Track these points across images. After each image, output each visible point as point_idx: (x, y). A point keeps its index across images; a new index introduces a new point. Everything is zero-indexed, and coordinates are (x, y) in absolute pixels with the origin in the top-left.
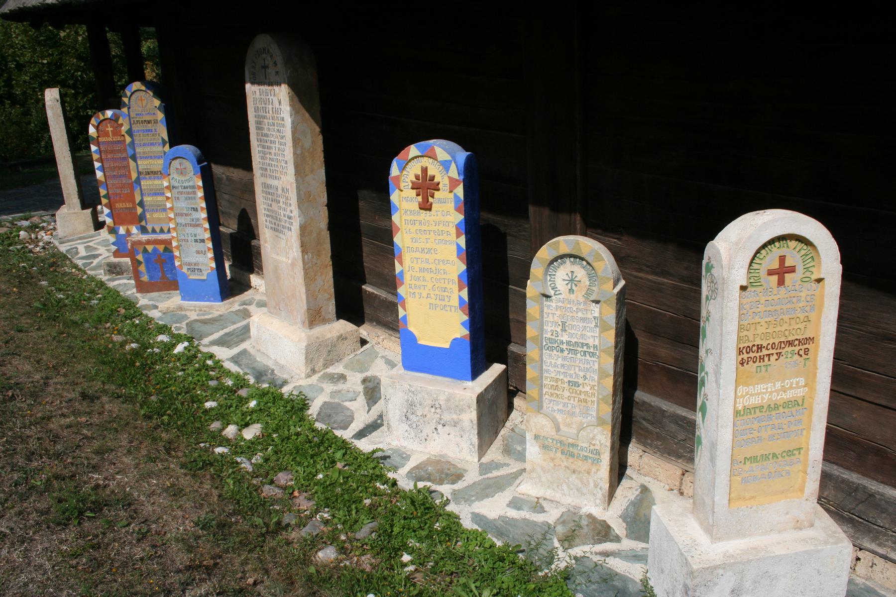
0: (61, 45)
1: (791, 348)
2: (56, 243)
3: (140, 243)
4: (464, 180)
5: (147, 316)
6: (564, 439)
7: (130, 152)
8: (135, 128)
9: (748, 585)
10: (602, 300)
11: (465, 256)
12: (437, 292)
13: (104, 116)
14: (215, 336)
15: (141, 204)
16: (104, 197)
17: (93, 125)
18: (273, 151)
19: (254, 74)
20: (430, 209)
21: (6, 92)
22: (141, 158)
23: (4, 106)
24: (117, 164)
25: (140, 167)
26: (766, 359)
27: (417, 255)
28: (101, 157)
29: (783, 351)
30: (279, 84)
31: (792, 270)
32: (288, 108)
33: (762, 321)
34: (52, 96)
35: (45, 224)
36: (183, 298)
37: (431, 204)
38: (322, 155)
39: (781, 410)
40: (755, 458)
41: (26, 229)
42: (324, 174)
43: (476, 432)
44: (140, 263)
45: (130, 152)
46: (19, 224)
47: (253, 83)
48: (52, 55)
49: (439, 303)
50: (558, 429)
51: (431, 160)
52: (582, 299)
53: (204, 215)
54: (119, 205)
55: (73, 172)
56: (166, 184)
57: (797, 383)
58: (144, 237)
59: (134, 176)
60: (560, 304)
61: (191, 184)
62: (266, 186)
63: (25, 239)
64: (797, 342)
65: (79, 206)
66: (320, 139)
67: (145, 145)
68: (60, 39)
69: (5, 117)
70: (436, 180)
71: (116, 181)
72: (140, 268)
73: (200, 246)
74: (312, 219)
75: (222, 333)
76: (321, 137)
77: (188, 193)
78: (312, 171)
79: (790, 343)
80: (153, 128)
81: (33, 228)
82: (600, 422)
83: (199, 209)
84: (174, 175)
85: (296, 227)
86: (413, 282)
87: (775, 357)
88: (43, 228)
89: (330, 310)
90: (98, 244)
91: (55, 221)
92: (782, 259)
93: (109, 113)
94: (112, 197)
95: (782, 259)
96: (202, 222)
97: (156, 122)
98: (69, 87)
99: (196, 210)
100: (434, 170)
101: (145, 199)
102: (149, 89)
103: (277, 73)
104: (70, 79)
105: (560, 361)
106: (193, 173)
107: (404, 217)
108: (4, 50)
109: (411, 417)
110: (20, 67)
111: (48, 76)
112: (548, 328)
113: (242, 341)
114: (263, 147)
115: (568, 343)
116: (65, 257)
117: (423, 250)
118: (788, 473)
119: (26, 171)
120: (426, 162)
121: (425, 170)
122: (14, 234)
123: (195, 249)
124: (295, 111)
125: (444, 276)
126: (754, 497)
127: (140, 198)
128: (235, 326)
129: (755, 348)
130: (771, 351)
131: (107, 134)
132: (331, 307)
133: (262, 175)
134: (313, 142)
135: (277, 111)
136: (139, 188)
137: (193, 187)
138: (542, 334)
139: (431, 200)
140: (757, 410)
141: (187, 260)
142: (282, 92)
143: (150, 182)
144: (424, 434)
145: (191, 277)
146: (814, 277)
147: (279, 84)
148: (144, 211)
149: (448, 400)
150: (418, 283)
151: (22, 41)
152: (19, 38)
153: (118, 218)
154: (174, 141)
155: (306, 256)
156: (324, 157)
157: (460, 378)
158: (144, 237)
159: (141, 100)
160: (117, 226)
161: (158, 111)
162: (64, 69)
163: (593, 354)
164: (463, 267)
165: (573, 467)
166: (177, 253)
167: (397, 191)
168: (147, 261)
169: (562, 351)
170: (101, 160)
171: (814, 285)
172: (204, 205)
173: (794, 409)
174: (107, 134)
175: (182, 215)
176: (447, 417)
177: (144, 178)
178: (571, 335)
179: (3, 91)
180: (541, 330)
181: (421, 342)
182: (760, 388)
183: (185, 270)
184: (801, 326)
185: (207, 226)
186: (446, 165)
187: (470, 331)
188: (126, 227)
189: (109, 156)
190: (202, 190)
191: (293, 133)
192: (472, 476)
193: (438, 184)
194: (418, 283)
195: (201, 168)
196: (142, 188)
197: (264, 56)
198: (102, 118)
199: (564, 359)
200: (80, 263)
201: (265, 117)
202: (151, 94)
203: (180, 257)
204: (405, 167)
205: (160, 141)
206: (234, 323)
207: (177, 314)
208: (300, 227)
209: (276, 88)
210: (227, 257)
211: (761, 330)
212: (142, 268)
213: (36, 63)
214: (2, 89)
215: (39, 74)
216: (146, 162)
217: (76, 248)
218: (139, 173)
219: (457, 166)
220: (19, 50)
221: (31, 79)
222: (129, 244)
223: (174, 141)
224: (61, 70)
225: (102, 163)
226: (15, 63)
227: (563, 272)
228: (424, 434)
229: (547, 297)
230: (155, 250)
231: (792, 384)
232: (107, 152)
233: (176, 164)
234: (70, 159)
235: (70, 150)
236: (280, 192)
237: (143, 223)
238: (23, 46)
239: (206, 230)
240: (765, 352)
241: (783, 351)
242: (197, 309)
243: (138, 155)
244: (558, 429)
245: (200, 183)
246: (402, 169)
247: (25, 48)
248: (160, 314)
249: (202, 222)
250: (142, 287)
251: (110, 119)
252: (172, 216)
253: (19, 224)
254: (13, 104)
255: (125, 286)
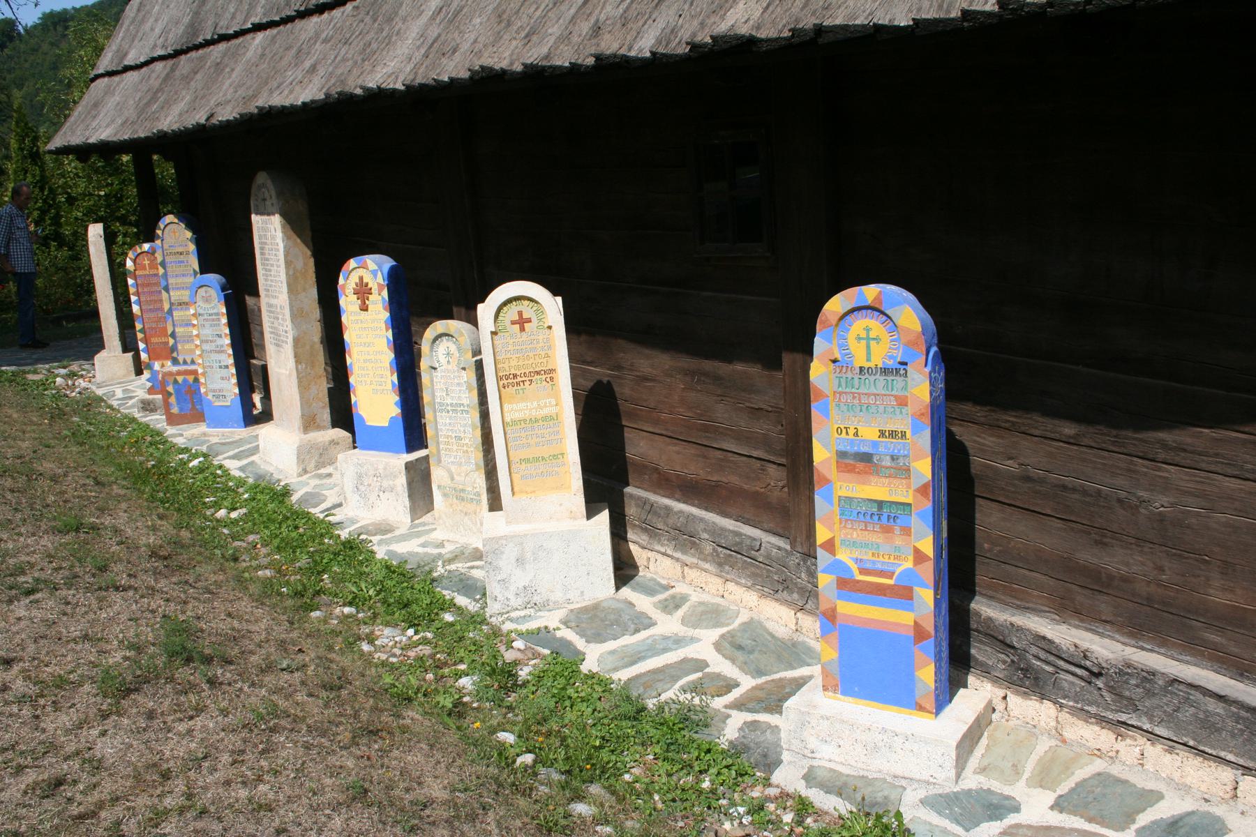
0: (124, 171)
1: (539, 377)
2: (94, 388)
3: (170, 374)
4: (388, 285)
5: (171, 442)
6: (456, 486)
7: (163, 283)
8: (168, 259)
9: (528, 555)
10: (467, 367)
11: (392, 347)
12: (376, 379)
13: (141, 249)
14: (231, 453)
15: (173, 335)
16: (140, 331)
17: (131, 259)
18: (272, 273)
19: (257, 206)
20: (367, 310)
21: (52, 232)
22: (173, 289)
23: (49, 248)
24: (152, 298)
25: (172, 298)
26: (522, 384)
27: (361, 348)
28: (138, 290)
29: (534, 379)
30: (273, 214)
31: (529, 321)
32: (281, 235)
33: (514, 357)
34: (95, 232)
35: (84, 373)
36: (209, 426)
37: (367, 306)
38: (314, 276)
39: (541, 423)
40: (528, 460)
41: (62, 377)
42: (316, 293)
43: (407, 495)
44: (170, 394)
45: (163, 283)
46: (56, 372)
47: (257, 214)
48: (112, 184)
49: (379, 388)
50: (452, 479)
51: (365, 270)
52: (456, 369)
53: (228, 341)
54: (155, 340)
55: (114, 312)
56: (192, 311)
57: (550, 403)
58: (175, 369)
59: (166, 307)
60: (443, 374)
61: (215, 311)
62: (270, 306)
63: (60, 385)
64: (543, 372)
65: (120, 349)
66: (311, 262)
67: (177, 276)
68: (122, 164)
69: (50, 262)
70: (369, 286)
71: (152, 315)
72: (170, 400)
73: (224, 372)
74: (305, 333)
75: (237, 451)
76: (312, 260)
77: (213, 320)
78: (304, 290)
79: (538, 373)
80: (185, 259)
81: (73, 375)
82: (478, 468)
83: (223, 335)
84: (200, 303)
85: (290, 340)
86: (360, 372)
87: (527, 383)
88: (82, 376)
89: (325, 418)
90: (137, 387)
91: (94, 370)
92: (520, 313)
93: (146, 246)
94: (148, 331)
95: (520, 313)
96: (226, 348)
97: (188, 253)
98: (131, 224)
99: (220, 336)
100: (368, 278)
101: (177, 330)
102: (181, 221)
103: (272, 204)
104: (132, 215)
105: (448, 421)
106: (217, 300)
107: (350, 318)
108: (53, 180)
109: (360, 487)
110: (71, 200)
111: (105, 212)
112: (438, 394)
113: (252, 455)
114: (266, 270)
115: (451, 404)
116: (101, 399)
117: (365, 344)
118: (557, 473)
119: (70, 325)
120: (361, 272)
121: (361, 278)
122: (50, 380)
123: (220, 376)
124: (287, 237)
125: (381, 365)
126: (534, 492)
127: (172, 330)
128: (251, 445)
129: (511, 376)
130: (524, 379)
131: (144, 268)
132: (326, 415)
133: (266, 296)
134: (305, 264)
135: (273, 238)
136: (171, 319)
137: (217, 314)
138: (434, 399)
139: (367, 302)
140: (522, 422)
141: (211, 386)
142: (276, 220)
143: (182, 313)
144: (370, 502)
145: (217, 404)
146: (546, 326)
147: (273, 214)
148: (176, 342)
149: (385, 469)
150: (363, 372)
151: (75, 168)
152: (73, 165)
153: (154, 355)
154: (204, 269)
155: (300, 366)
156: (316, 278)
157: (398, 452)
158: (175, 369)
159: (174, 232)
160: (152, 362)
161: (190, 243)
162: (125, 202)
163: (467, 412)
164: (392, 356)
165: (465, 510)
166: (202, 380)
167: (344, 296)
168: (178, 392)
169: (448, 412)
170: (137, 294)
171: (547, 331)
172: (227, 331)
173: (551, 423)
174: (144, 268)
175: (207, 341)
176: (385, 484)
177: (176, 309)
178: (452, 398)
179: (50, 230)
180: (433, 396)
181: (369, 423)
182: (522, 405)
183: (210, 397)
184: (545, 360)
185: (230, 352)
186: (374, 273)
187: (402, 410)
188: (160, 362)
189: (146, 290)
190: (226, 316)
191: (286, 256)
192: (403, 530)
193: (371, 289)
194: (363, 372)
195: (225, 295)
196: (175, 319)
197: (263, 190)
198: (139, 251)
199: (450, 418)
200: (115, 403)
201: (266, 243)
202: (184, 226)
203: (205, 384)
204: (348, 277)
205: (192, 272)
206: (250, 443)
207: (198, 440)
208: (294, 340)
209: (272, 217)
210: (259, 390)
211: (513, 363)
212: (173, 400)
213: (91, 195)
214: (48, 228)
215: (94, 208)
216: (178, 293)
217: (114, 391)
218: (172, 304)
219: (382, 274)
220: (72, 179)
221: (84, 215)
222: (160, 376)
223: (204, 269)
224: (121, 204)
225: (139, 297)
226: (65, 196)
227: (444, 346)
228: (370, 502)
229: (435, 369)
230: (185, 381)
231: (546, 403)
232: (143, 285)
233: (202, 292)
234: (112, 298)
235: (113, 289)
236: (279, 310)
237: (175, 355)
238: (77, 174)
239: (229, 355)
240: (519, 379)
241: (534, 379)
242: (220, 434)
243: (170, 287)
244: (452, 479)
245: (224, 310)
246: (347, 278)
247: (79, 177)
248: (185, 440)
249: (226, 348)
250: (172, 420)
251: (147, 252)
252: (198, 342)
253: (56, 372)
254: (60, 246)
255: (157, 420)
